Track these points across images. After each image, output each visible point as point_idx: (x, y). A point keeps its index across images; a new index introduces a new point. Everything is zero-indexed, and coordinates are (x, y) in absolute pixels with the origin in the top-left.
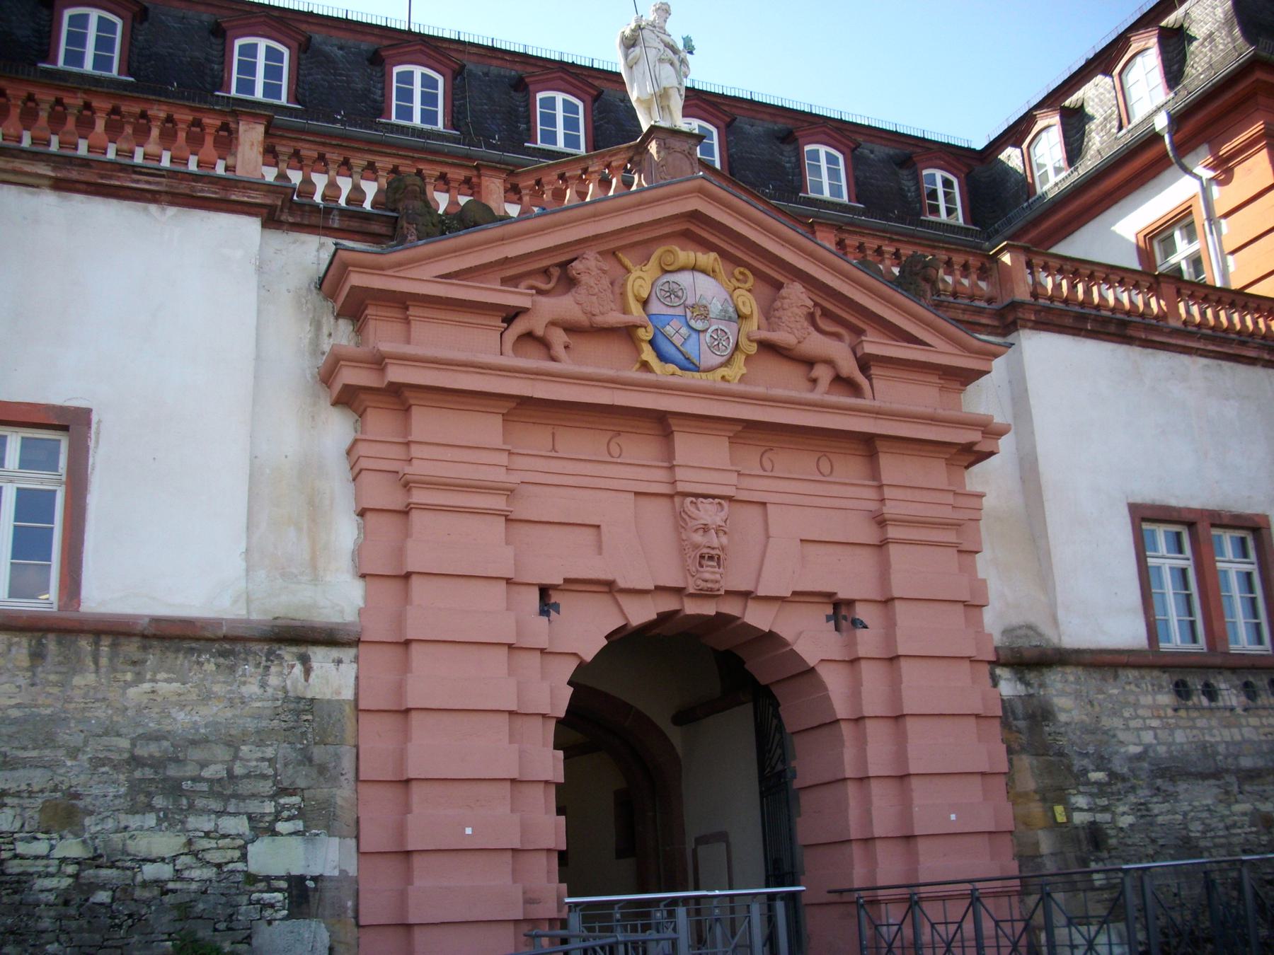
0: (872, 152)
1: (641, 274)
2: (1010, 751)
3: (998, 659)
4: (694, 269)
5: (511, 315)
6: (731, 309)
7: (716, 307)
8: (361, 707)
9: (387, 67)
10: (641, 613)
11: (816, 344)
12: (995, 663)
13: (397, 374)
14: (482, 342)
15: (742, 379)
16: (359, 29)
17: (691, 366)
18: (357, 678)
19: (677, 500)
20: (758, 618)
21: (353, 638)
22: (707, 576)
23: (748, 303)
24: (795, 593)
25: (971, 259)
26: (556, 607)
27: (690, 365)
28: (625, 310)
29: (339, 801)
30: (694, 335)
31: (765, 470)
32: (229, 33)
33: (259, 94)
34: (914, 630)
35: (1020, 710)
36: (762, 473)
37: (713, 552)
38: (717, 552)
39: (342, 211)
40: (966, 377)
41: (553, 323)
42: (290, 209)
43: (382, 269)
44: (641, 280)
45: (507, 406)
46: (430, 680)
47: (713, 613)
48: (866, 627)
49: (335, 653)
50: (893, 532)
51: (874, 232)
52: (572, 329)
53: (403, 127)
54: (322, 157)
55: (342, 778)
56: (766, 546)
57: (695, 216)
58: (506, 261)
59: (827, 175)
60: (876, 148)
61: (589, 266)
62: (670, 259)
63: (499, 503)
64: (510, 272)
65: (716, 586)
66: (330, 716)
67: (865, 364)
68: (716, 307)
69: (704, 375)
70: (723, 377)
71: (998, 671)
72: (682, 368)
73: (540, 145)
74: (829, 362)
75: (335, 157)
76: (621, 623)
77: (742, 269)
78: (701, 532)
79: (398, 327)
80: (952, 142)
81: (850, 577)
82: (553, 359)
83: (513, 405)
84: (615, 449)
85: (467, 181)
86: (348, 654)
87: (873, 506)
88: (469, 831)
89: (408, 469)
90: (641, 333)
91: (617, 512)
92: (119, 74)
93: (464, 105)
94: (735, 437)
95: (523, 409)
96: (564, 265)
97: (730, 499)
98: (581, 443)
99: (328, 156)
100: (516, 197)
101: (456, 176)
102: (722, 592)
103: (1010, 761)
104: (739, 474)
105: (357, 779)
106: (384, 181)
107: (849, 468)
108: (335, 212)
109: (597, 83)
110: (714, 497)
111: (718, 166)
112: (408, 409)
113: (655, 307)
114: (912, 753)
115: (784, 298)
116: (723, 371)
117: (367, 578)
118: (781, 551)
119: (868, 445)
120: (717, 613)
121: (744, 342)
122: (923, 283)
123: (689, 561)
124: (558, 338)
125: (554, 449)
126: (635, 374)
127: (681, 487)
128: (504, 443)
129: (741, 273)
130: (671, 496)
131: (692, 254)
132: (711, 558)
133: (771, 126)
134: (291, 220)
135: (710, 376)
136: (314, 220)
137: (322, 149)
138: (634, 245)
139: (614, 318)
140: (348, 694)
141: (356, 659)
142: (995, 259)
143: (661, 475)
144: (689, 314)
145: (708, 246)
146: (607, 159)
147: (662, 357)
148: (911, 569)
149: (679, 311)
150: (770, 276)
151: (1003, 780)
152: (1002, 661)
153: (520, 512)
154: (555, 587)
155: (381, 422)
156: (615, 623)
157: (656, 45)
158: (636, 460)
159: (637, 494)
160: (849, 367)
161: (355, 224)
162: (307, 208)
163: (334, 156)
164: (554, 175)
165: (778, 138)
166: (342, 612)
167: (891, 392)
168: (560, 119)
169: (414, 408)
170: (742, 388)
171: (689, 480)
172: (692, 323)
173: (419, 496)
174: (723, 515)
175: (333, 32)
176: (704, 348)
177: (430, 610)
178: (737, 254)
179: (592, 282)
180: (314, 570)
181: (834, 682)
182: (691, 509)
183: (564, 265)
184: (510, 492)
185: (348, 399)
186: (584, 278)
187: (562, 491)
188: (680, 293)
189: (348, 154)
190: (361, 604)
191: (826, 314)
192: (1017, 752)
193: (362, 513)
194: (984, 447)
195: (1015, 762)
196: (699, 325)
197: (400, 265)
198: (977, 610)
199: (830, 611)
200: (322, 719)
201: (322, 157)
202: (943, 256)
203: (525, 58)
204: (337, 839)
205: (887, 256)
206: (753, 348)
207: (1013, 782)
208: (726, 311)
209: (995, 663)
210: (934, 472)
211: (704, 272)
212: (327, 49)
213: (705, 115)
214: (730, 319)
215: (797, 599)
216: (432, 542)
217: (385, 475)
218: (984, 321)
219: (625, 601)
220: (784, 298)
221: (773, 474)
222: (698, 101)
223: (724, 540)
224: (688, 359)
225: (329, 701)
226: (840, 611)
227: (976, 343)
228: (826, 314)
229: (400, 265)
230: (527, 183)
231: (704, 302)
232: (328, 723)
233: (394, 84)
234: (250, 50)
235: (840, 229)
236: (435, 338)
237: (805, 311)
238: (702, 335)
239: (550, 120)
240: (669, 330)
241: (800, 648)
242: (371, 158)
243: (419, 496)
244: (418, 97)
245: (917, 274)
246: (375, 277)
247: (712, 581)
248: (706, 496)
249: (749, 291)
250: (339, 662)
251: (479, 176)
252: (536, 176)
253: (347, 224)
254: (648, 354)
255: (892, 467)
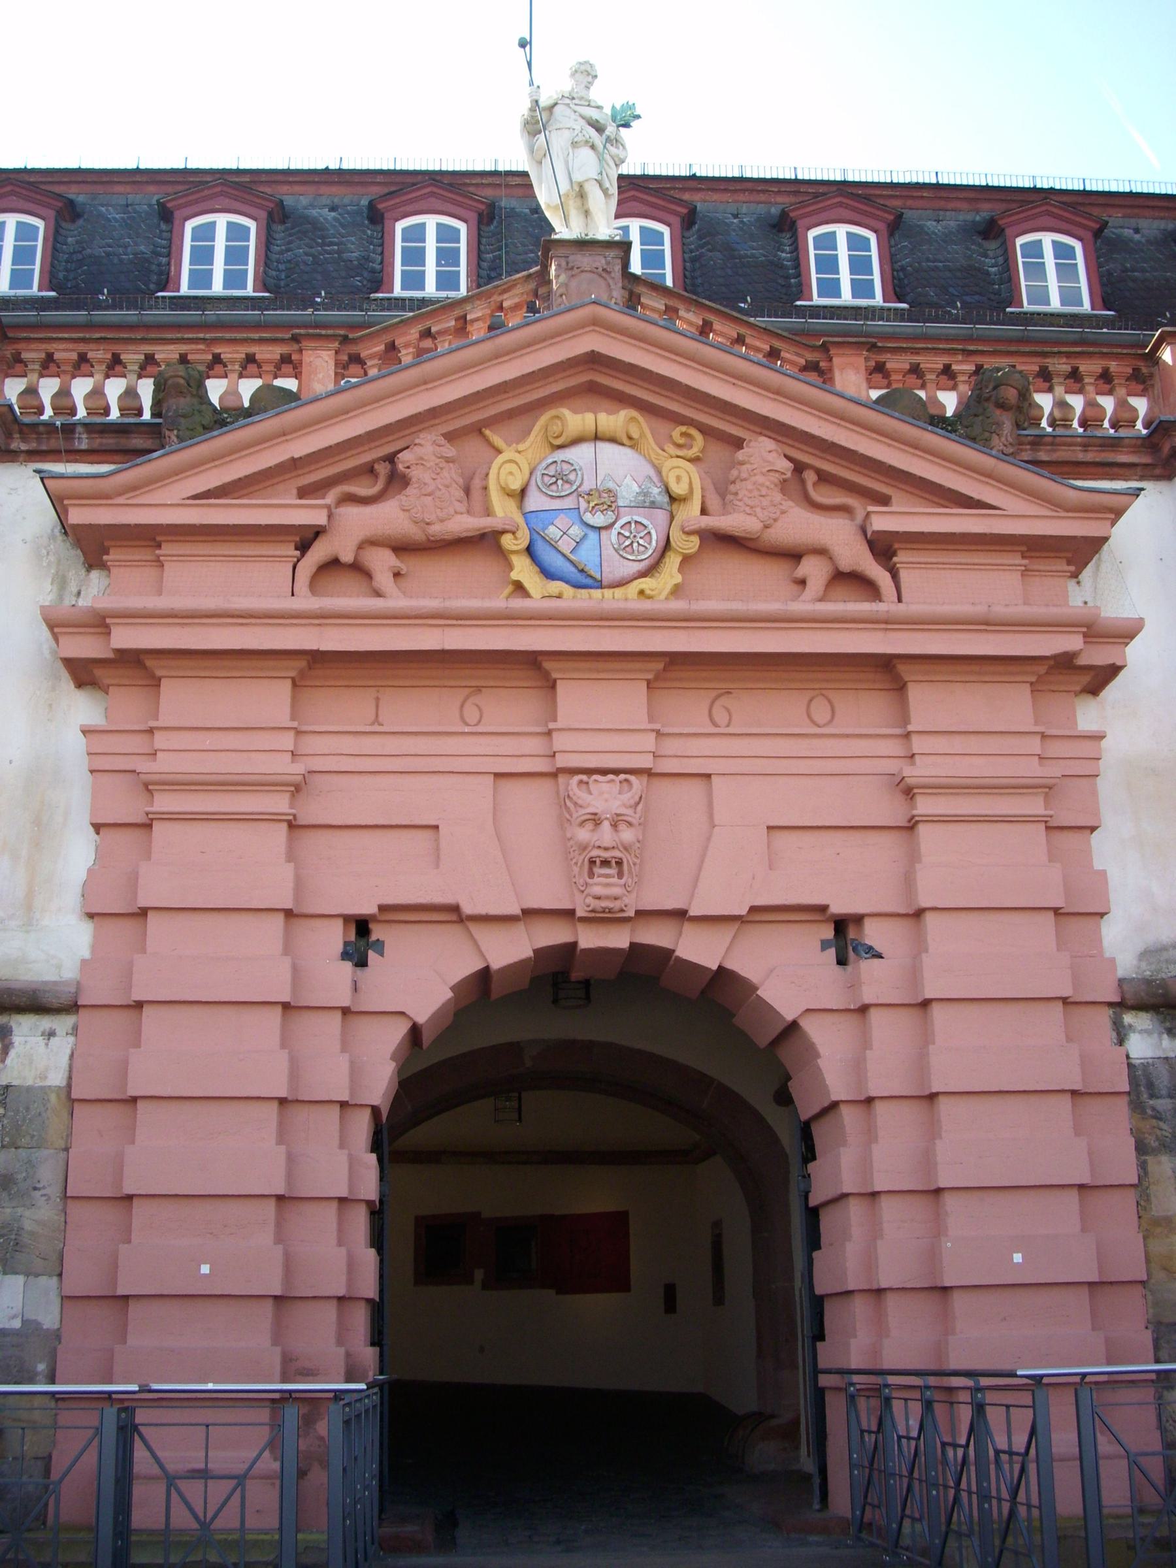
0: (1137, 231)
1: (517, 457)
2: (1141, 1148)
3: (1123, 998)
4: (597, 438)
5: (306, 538)
6: (656, 491)
7: (628, 491)
8: (74, 1096)
9: (387, 223)
10: (508, 950)
11: (797, 524)
12: (1121, 1006)
13: (125, 638)
14: (262, 584)
15: (677, 591)
16: (356, 179)
17: (589, 581)
18: (72, 1056)
19: (561, 779)
20: (700, 950)
21: (65, 1000)
22: (598, 890)
23: (684, 476)
24: (753, 909)
25: (1113, 366)
26: (379, 947)
27: (585, 580)
28: (488, 512)
29: (28, 1225)
30: (593, 536)
31: (716, 725)
32: (800, 224)
33: (430, 289)
34: (954, 958)
35: (1163, 1080)
36: (716, 730)
37: (606, 855)
38: (617, 854)
39: (89, 427)
40: (1079, 553)
41: (371, 542)
42: (21, 432)
43: (108, 497)
44: (511, 463)
45: (294, 667)
46: (164, 1057)
47: (625, 945)
48: (880, 956)
49: (46, 1022)
50: (925, 806)
51: (931, 344)
52: (402, 548)
53: (411, 300)
54: (83, 358)
55: (37, 1194)
56: (709, 839)
57: (594, 359)
58: (294, 465)
59: (844, 265)
60: (1143, 224)
61: (425, 455)
62: (556, 428)
63: (1034, 806)
64: (308, 475)
65: (616, 905)
66: (27, 1109)
67: (884, 548)
68: (628, 491)
69: (608, 593)
70: (642, 592)
71: (1128, 1018)
72: (578, 586)
73: (817, 300)
74: (821, 552)
75: (100, 355)
76: (480, 966)
77: (684, 429)
78: (590, 825)
79: (150, 573)
80: (995, 182)
81: (851, 879)
82: (378, 594)
83: (661, 666)
84: (720, 716)
85: (286, 359)
86: (68, 1021)
87: (891, 766)
88: (205, 1269)
89: (908, 771)
90: (507, 541)
91: (463, 805)
92: (40, 290)
93: (500, 258)
94: (657, 678)
95: (315, 668)
96: (391, 459)
97: (648, 773)
98: (414, 709)
99: (90, 355)
100: (951, 383)
101: (268, 356)
102: (632, 914)
103: (1143, 1166)
104: (1044, 736)
105: (65, 1197)
106: (965, 389)
107: (863, 710)
108: (79, 429)
109: (686, 196)
110: (616, 772)
111: (669, 282)
112: (553, 686)
113: (535, 501)
114: (943, 1150)
115: (742, 463)
116: (645, 583)
117: (96, 918)
118: (740, 848)
119: (888, 671)
120: (633, 945)
121: (676, 537)
122: (998, 412)
123: (576, 870)
124: (382, 562)
125: (376, 721)
126: (500, 601)
127: (562, 761)
128: (1036, 723)
129: (683, 434)
130: (554, 775)
131: (589, 417)
132: (605, 863)
133: (969, 217)
134: (24, 447)
135: (619, 592)
136: (58, 443)
137: (82, 347)
138: (510, 415)
139: (464, 523)
140: (57, 1079)
141: (75, 1031)
142: (1153, 358)
143: (534, 745)
144: (583, 505)
145: (623, 400)
146: (496, 298)
147: (548, 574)
148: (952, 863)
149: (569, 503)
150: (722, 429)
151: (1131, 1197)
152: (1129, 1003)
153: (312, 812)
154: (373, 918)
155: (128, 704)
156: (469, 966)
157: (571, 124)
158: (502, 725)
159: (497, 775)
160: (854, 554)
161: (109, 441)
162: (41, 429)
163: (99, 354)
164: (414, 332)
165: (979, 233)
166: (59, 967)
167: (929, 587)
168: (429, 254)
169: (558, 682)
170: (678, 606)
171: (574, 749)
172: (588, 518)
173: (165, 802)
174: (629, 797)
175: (324, 189)
176: (609, 552)
177: (172, 960)
178: (662, 404)
179: (426, 477)
180: (28, 911)
181: (830, 1044)
182: (580, 794)
183: (391, 459)
184: (1047, 789)
185: (83, 673)
186: (415, 473)
187: (378, 779)
188: (572, 477)
189: (117, 348)
190: (86, 954)
191: (824, 478)
192: (1155, 1152)
193: (97, 827)
194: (1098, 656)
195: (1150, 1168)
196: (598, 520)
197: (134, 488)
198: (1088, 923)
199: (828, 932)
200: (17, 1111)
201: (83, 358)
202: (939, 362)
203: (794, 186)
204: (20, 1279)
205: (961, 378)
206: (693, 544)
207: (1148, 1200)
208: (646, 494)
209: (1121, 1006)
210: (1013, 706)
211: (613, 440)
212: (314, 212)
213: (857, 217)
214: (653, 505)
215: (757, 917)
216: (180, 864)
217: (122, 775)
218: (1123, 458)
219: (483, 934)
220: (742, 463)
221: (730, 730)
222: (640, 192)
223: (627, 835)
224: (582, 571)
225: (29, 1089)
226: (845, 935)
227: (1072, 494)
228: (824, 478)
229: (134, 488)
230: (372, 349)
231: (611, 485)
232: (24, 1119)
233: (1020, 260)
234: (828, 241)
235: (873, 347)
236: (192, 580)
237: (775, 477)
238: (603, 533)
239: (829, 264)
240: (553, 532)
241: (766, 993)
242: (148, 348)
243: (165, 802)
244: (218, 256)
245: (988, 399)
246: (101, 510)
247: (607, 898)
248: (604, 772)
249: (694, 460)
250: (51, 1034)
251: (301, 351)
252: (387, 338)
253: (98, 442)
254: (523, 570)
255: (928, 703)
